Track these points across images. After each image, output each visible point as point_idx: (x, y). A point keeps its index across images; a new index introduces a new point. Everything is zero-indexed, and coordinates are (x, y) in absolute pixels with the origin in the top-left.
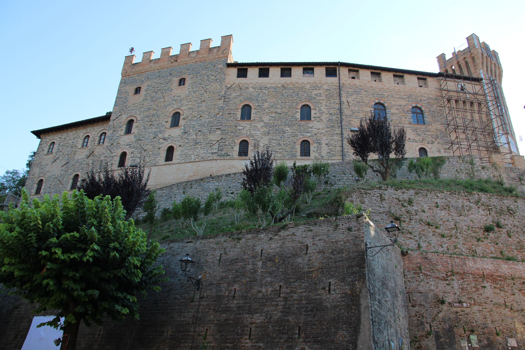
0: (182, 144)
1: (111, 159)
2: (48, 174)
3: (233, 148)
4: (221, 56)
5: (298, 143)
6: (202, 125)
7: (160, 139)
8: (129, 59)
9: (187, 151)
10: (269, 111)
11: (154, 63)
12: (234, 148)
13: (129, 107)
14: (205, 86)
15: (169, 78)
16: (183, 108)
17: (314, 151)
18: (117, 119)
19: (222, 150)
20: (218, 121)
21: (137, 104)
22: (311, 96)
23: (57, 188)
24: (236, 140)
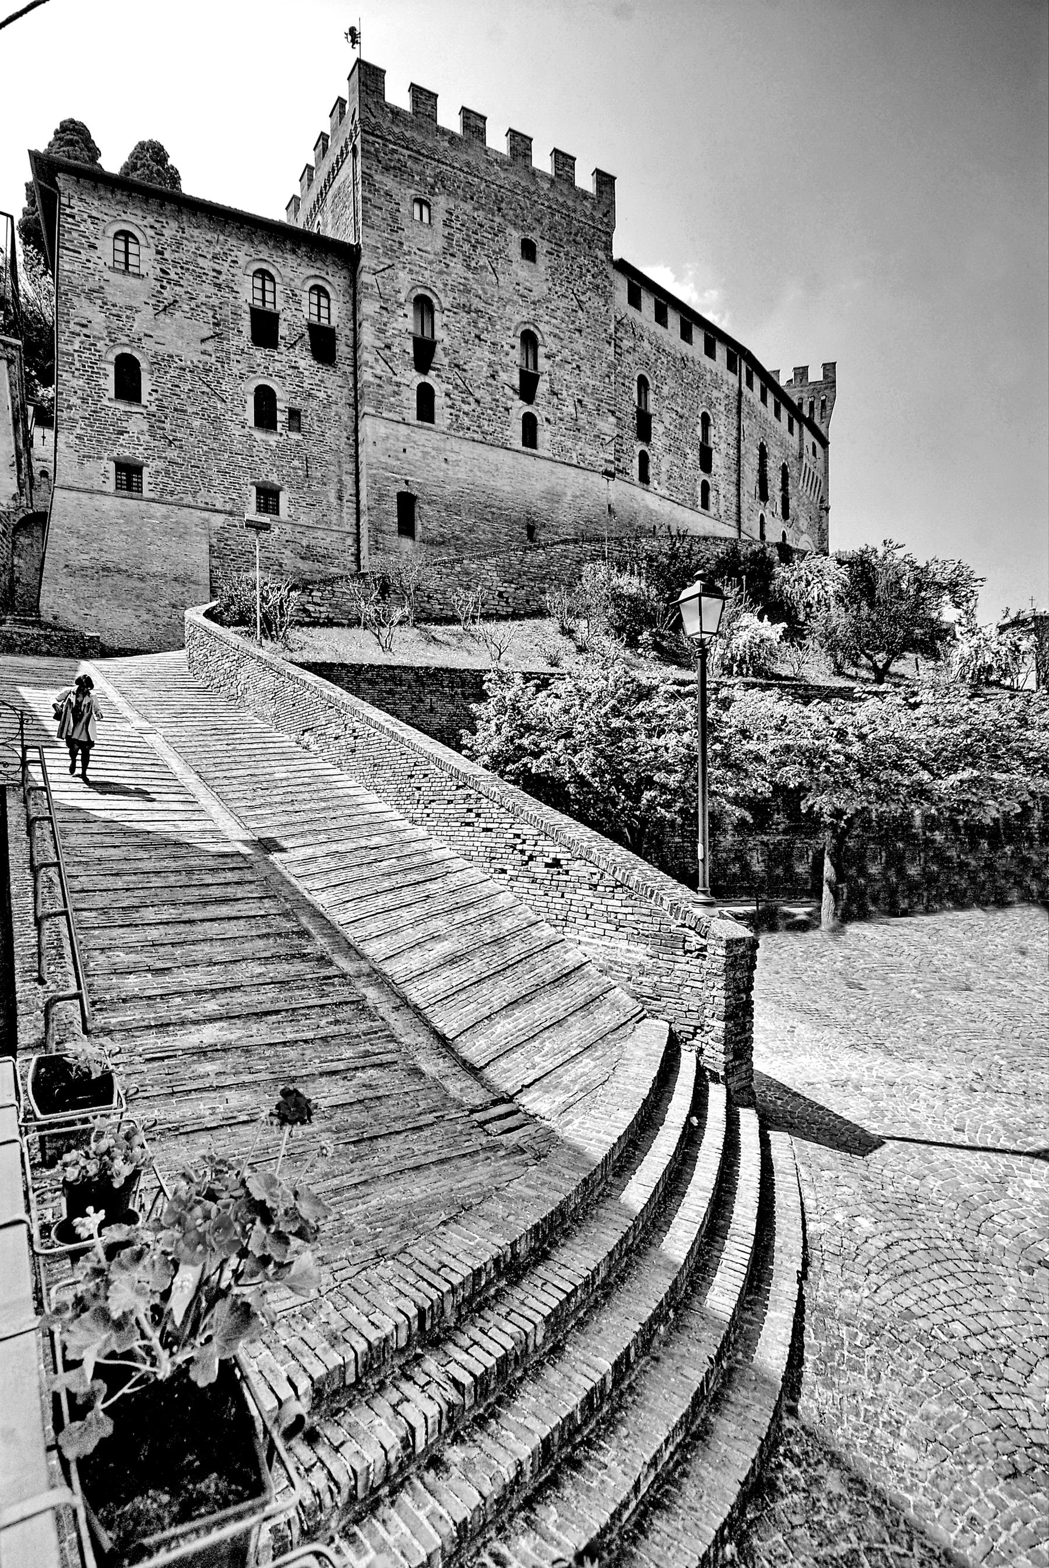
16: (541, 326)
23: (205, 405)
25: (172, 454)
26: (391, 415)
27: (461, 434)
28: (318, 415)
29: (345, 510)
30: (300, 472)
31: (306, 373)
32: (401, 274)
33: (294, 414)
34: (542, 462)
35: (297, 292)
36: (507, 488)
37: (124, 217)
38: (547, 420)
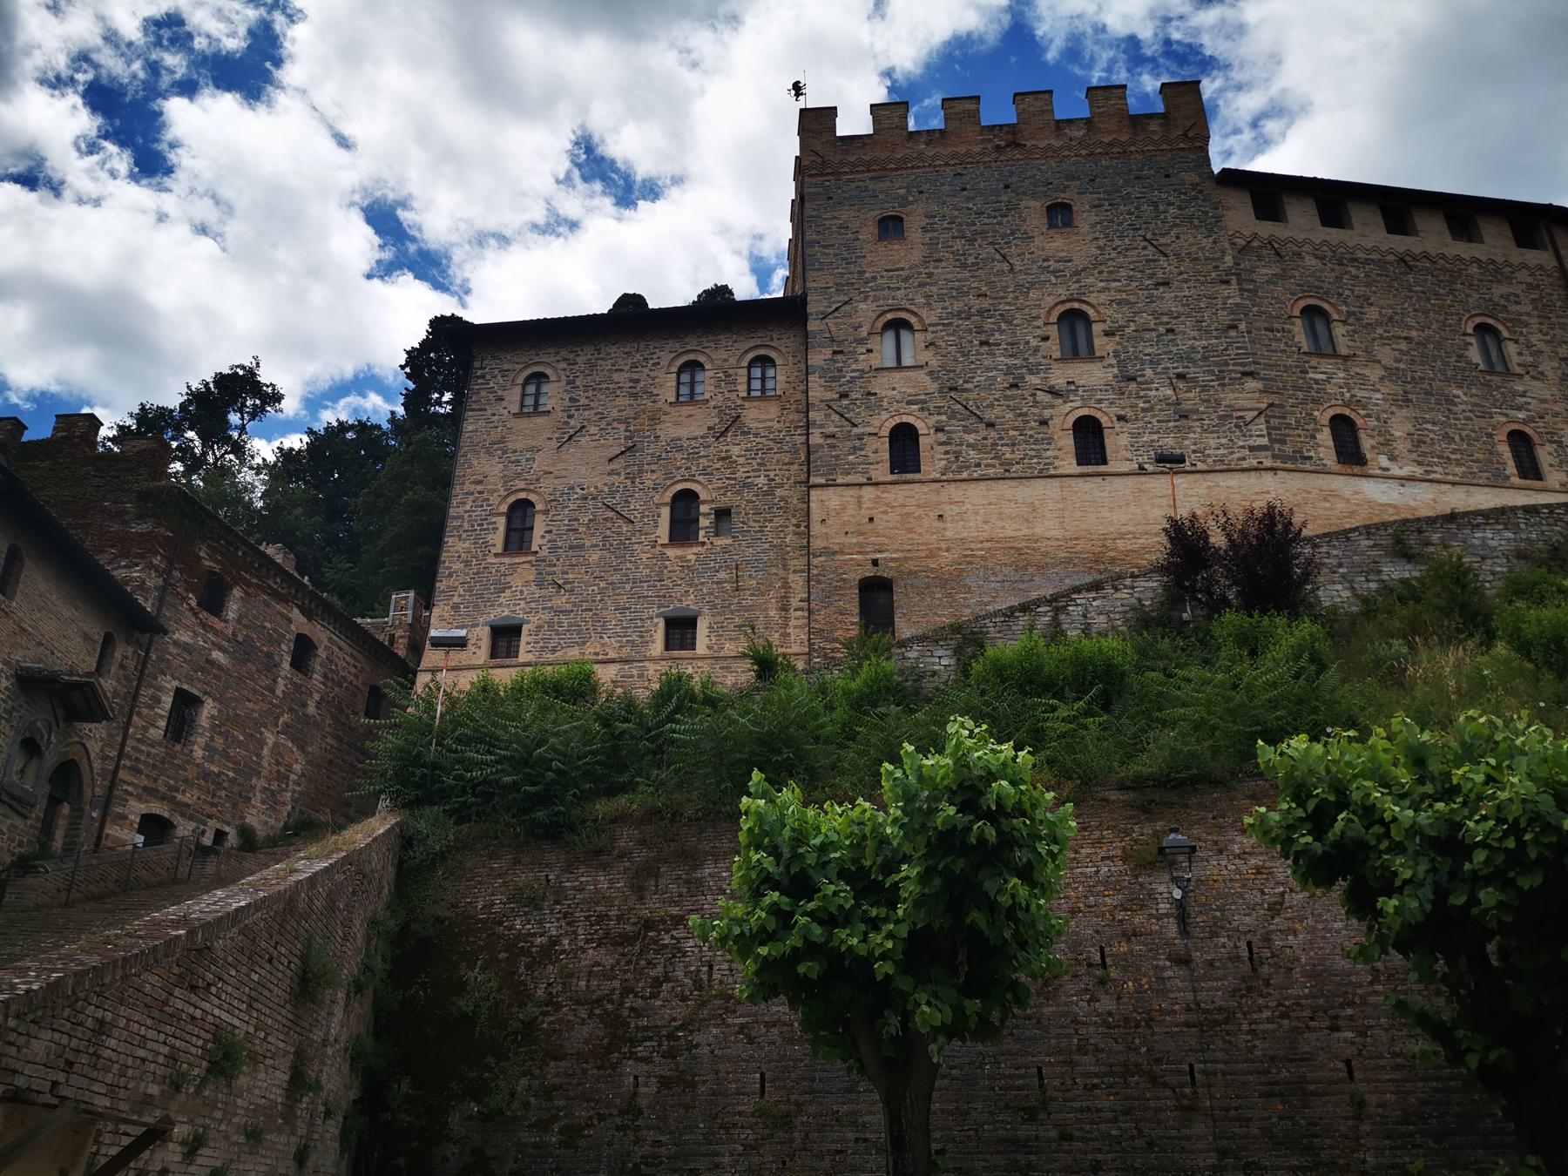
0: (1130, 414)
1: (857, 443)
2: (547, 485)
3: (1313, 437)
4: (1182, 145)
5: (1501, 438)
6: (1186, 358)
7: (1038, 393)
8: (816, 123)
9: (1155, 437)
10: (1386, 331)
11: (927, 144)
12: (1318, 436)
13: (874, 278)
14: (1154, 234)
15: (1005, 198)
16: (1092, 299)
17: (1551, 465)
18: (836, 314)
19: (1284, 442)
20: (1238, 348)
21: (902, 269)
22: (1491, 300)
23: (608, 533)
24: (1316, 413)
25: (561, 601)
26: (850, 479)
27: (965, 475)
28: (755, 508)
29: (793, 623)
30: (727, 586)
31: (741, 460)
32: (862, 306)
33: (723, 514)
34: (1116, 480)
35: (731, 371)
36: (1057, 533)
37: (537, 359)
38: (1121, 418)
